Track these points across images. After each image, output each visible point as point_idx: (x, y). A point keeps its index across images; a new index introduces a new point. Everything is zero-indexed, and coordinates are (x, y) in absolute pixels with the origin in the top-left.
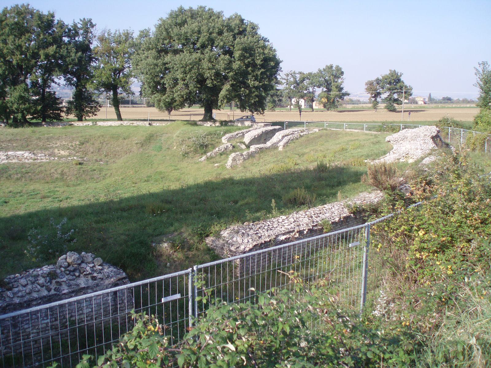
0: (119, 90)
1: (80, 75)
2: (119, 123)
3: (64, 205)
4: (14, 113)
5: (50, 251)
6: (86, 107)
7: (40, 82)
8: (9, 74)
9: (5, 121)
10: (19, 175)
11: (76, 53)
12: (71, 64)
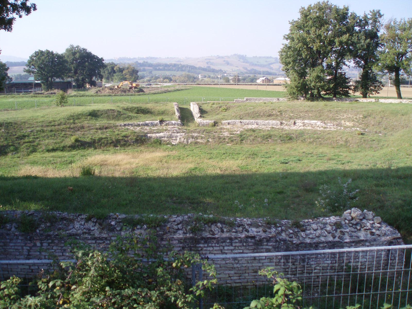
0: (401, 72)
1: (367, 59)
2: (398, 101)
3: (347, 167)
4: (312, 89)
5: (336, 205)
6: (371, 86)
7: (333, 64)
8: (310, 58)
9: (304, 95)
10: (312, 140)
11: (365, 40)
12: (360, 49)
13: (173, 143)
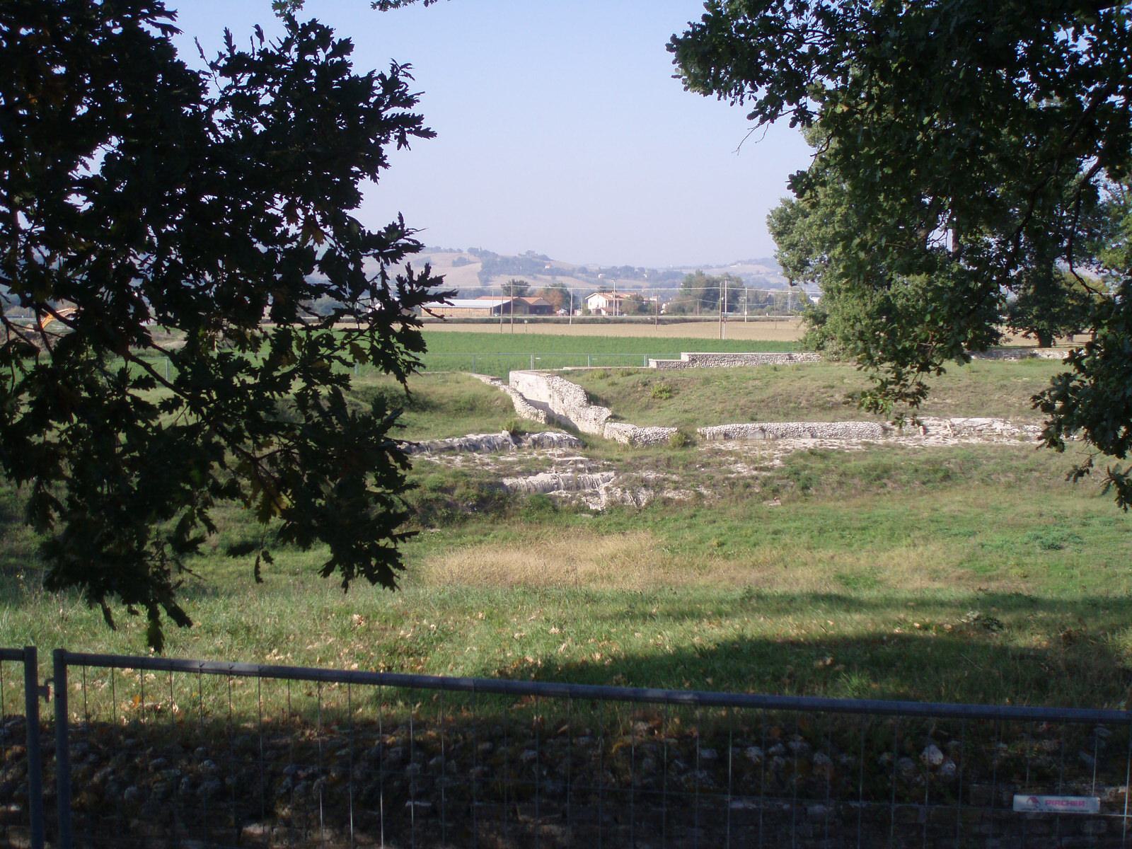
13: (592, 507)
